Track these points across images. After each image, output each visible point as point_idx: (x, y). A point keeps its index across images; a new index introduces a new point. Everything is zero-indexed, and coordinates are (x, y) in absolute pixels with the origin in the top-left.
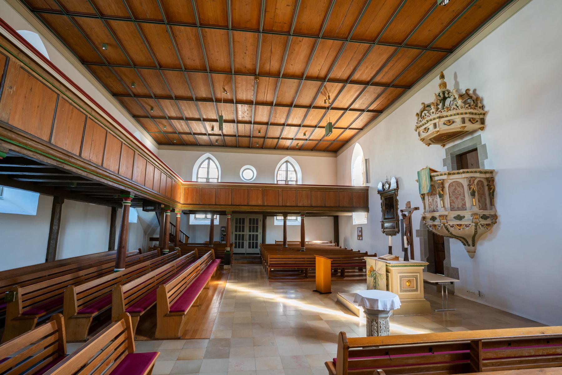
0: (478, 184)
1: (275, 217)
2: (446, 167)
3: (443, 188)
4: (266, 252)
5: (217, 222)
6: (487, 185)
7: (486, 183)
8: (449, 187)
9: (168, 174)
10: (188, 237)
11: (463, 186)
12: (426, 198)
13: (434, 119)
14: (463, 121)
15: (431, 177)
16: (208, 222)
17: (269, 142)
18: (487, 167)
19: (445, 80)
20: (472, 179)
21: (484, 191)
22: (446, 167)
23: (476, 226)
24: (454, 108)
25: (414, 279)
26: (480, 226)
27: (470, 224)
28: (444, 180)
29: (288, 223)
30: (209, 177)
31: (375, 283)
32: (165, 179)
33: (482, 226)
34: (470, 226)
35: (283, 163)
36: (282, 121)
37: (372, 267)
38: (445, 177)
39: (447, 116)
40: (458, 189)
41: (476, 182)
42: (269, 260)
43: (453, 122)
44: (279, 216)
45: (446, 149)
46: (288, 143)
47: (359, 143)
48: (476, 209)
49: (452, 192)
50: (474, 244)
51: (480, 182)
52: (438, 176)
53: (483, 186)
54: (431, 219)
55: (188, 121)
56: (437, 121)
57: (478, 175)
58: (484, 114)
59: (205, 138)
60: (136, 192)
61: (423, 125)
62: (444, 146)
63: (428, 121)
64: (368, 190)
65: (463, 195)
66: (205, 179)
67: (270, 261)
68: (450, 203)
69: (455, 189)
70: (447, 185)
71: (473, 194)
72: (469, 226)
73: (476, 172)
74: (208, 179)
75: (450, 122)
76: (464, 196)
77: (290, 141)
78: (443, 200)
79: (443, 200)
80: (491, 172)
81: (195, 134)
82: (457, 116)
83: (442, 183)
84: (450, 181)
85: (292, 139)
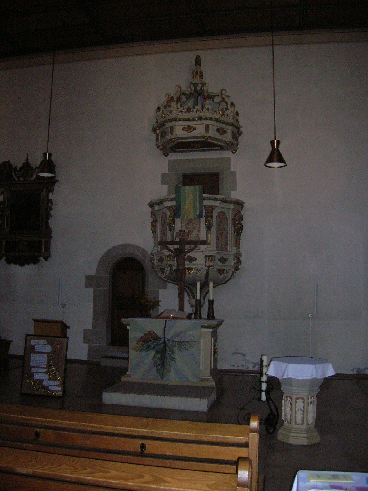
2: (166, 187)
4: (92, 471)
13: (211, 119)
18: (234, 195)
19: (202, 68)
22: (166, 187)
24: (197, 109)
27: (202, 268)
31: (284, 372)
34: (202, 270)
42: (254, 439)
43: (195, 129)
45: (169, 161)
49: (185, 225)
54: (220, 260)
57: (217, 203)
61: (189, 120)
63: (200, 118)
65: (198, 230)
67: (246, 445)
70: (215, 214)
73: (214, 199)
74: (272, 36)
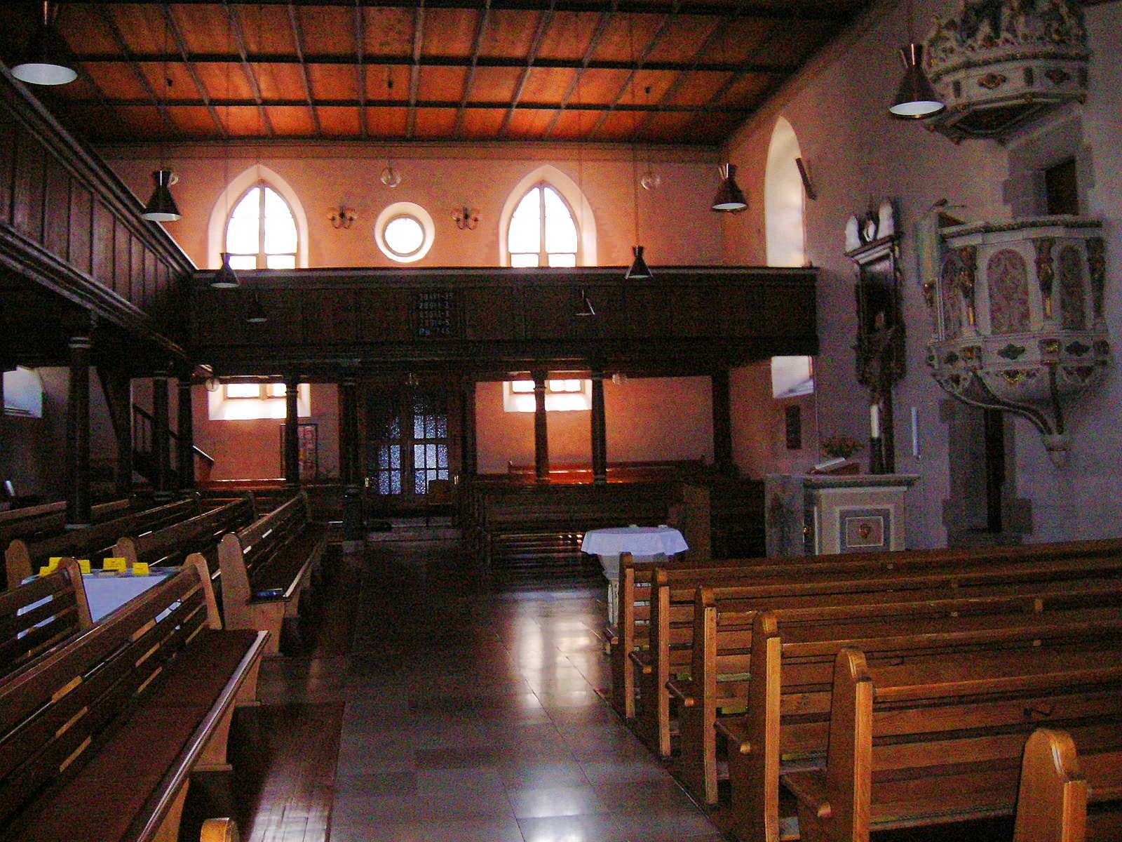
0: (1062, 259)
1: (506, 384)
3: (972, 268)
5: (304, 410)
6: (1089, 260)
7: (1084, 256)
8: (990, 268)
9: (159, 253)
10: (210, 463)
11: (1023, 265)
12: (938, 296)
14: (1029, 77)
15: (943, 239)
16: (278, 411)
17: (477, 118)
20: (1046, 244)
21: (1078, 277)
23: (1053, 374)
25: (879, 520)
26: (1064, 373)
27: (1037, 370)
28: (974, 248)
29: (551, 404)
30: (266, 252)
32: (152, 269)
33: (1070, 373)
35: (530, 189)
36: (519, 52)
37: (776, 499)
38: (976, 240)
39: (987, 63)
40: (1013, 272)
41: (1055, 254)
43: (1004, 80)
44: (519, 378)
46: (540, 119)
47: (787, 116)
48: (1052, 328)
50: (1060, 426)
51: (1070, 254)
52: (959, 235)
53: (1077, 263)
55: (197, 63)
56: (960, 75)
58: (1085, 58)
59: (249, 112)
60: (102, 313)
62: (1002, 142)
64: (813, 278)
66: (254, 258)
68: (992, 311)
69: (1006, 272)
70: (982, 264)
71: (1046, 287)
72: (1034, 374)
75: (993, 81)
76: (1026, 293)
77: (550, 113)
78: (972, 305)
79: (972, 305)
80: (1097, 225)
81: (215, 102)
82: (1010, 65)
83: (971, 255)
84: (991, 252)
85: (557, 106)
